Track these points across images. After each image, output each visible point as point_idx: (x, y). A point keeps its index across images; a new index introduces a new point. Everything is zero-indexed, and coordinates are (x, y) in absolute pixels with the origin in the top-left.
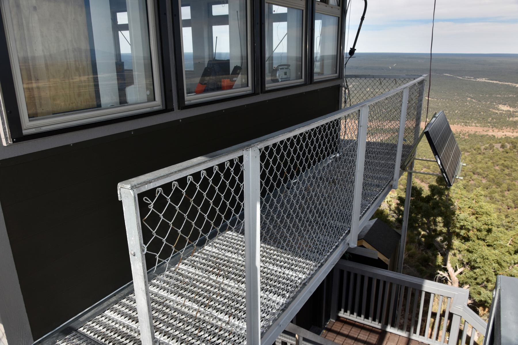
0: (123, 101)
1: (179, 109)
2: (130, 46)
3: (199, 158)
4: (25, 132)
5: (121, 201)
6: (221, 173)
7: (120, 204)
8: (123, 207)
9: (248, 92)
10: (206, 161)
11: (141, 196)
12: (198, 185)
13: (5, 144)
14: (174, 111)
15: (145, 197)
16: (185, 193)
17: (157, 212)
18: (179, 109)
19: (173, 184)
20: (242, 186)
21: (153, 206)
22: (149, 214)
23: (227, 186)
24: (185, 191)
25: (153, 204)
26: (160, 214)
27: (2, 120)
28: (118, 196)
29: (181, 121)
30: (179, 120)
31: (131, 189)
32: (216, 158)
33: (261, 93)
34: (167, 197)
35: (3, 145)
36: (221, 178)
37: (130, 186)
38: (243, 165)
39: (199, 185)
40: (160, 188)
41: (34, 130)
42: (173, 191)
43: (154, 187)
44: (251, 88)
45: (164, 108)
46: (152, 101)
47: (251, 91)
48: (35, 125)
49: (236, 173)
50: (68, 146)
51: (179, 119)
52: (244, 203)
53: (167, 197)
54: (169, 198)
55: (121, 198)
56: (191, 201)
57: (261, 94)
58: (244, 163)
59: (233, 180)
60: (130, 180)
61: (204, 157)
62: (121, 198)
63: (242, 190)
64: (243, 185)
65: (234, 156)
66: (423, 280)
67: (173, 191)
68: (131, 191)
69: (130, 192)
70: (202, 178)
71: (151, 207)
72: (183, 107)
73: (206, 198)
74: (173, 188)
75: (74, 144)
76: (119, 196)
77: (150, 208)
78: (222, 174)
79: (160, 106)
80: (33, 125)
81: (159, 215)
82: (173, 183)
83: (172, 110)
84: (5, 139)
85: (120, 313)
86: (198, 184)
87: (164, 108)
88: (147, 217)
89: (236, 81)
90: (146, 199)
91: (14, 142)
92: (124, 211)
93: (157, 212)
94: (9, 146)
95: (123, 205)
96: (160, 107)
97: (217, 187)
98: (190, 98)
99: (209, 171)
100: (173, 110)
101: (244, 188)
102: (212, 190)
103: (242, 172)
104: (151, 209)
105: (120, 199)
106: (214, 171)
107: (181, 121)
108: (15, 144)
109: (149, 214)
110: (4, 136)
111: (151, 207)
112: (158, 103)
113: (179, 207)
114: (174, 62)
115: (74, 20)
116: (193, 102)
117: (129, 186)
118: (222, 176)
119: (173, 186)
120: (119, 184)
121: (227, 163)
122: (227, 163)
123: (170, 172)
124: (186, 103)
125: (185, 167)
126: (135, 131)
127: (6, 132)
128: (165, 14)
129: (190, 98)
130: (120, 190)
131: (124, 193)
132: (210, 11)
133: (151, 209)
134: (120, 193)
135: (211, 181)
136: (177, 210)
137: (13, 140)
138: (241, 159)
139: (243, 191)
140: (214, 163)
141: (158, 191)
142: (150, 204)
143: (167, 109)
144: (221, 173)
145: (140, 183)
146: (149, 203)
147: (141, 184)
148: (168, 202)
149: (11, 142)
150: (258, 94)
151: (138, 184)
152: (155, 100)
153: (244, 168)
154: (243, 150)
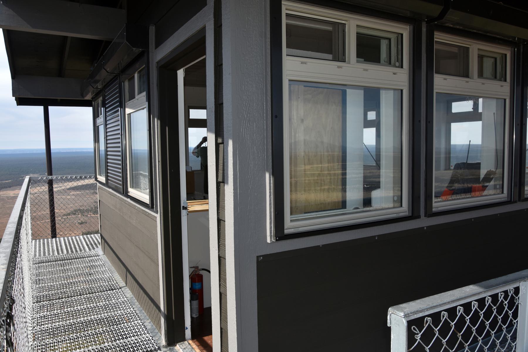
0: (367, 202)
1: (425, 216)
2: (364, 142)
3: (471, 287)
4: (286, 232)
5: (390, 328)
6: (493, 306)
7: (388, 330)
8: (392, 334)
9: (502, 199)
10: (481, 292)
11: (410, 323)
12: (468, 318)
13: (269, 241)
14: (420, 218)
15: (414, 326)
16: (453, 325)
17: (423, 344)
18: (425, 216)
19: (442, 315)
20: (515, 323)
21: (420, 337)
22: (415, 345)
23: (498, 322)
24: (454, 324)
25: (421, 335)
26: (426, 347)
27: (270, 220)
28: (388, 321)
29: (425, 228)
30: (424, 227)
31: (404, 317)
32: (492, 289)
33: (519, 200)
34: (435, 329)
35: (267, 241)
36: (493, 312)
37: (403, 314)
38: (519, 298)
39: (469, 318)
40: (429, 318)
41: (293, 230)
42: (442, 322)
43: (423, 315)
44: (507, 195)
45: (410, 215)
46: (399, 207)
47: (506, 199)
48: (294, 226)
49: (510, 308)
50: (319, 246)
51: (424, 226)
52: (516, 344)
53: (435, 329)
54: (438, 330)
55: (390, 324)
56: (458, 335)
57: (518, 203)
58: (520, 295)
59: (506, 316)
60: (401, 305)
61: (477, 286)
62: (390, 324)
63: (515, 328)
64: (517, 322)
65: (510, 288)
66: (190, 149)
67: (442, 322)
68: (403, 319)
69: (403, 321)
70: (474, 310)
71: (418, 337)
72: (430, 214)
73: (475, 335)
74: (442, 319)
75: (323, 245)
76: (388, 321)
77: (417, 338)
78: (495, 307)
79: (406, 212)
80: (293, 226)
81: (425, 348)
82: (442, 313)
83: (419, 217)
84: (269, 237)
85: (84, 239)
86: (468, 316)
87: (410, 215)
88: (412, 348)
89: (488, 186)
90: (414, 328)
91: (276, 240)
92: (392, 339)
93: (423, 344)
94: (272, 243)
95: (392, 333)
96: (407, 214)
97: (488, 322)
98: (438, 204)
99: (481, 302)
100: (419, 217)
101: (518, 326)
102: (483, 325)
103: (517, 306)
104: (417, 340)
105: (389, 325)
106: (486, 303)
107: (425, 228)
108: (277, 242)
109: (415, 345)
110: (269, 234)
111: (418, 337)
112: (405, 209)
113: (446, 341)
114: (424, 168)
115: (332, 128)
116: (441, 209)
117: (402, 314)
118: (494, 309)
119: (442, 317)
120: (390, 309)
121: (502, 295)
122: (502, 295)
123: (443, 302)
124: (433, 209)
125: (459, 298)
126: (379, 236)
127: (272, 230)
128: (420, 121)
129: (438, 204)
130: (391, 315)
131: (395, 319)
132: (450, 108)
133: (417, 340)
134: (391, 319)
135: (482, 314)
136: (443, 345)
137: (276, 238)
138: (517, 290)
139: (516, 330)
140: (487, 295)
141: (426, 320)
142: (418, 334)
143: (414, 215)
144: (493, 306)
145: (413, 311)
146: (417, 333)
147: (414, 312)
148: (436, 334)
149: (274, 240)
150: (515, 202)
151: (411, 313)
152: (401, 206)
153: (520, 301)
154: (520, 282)
